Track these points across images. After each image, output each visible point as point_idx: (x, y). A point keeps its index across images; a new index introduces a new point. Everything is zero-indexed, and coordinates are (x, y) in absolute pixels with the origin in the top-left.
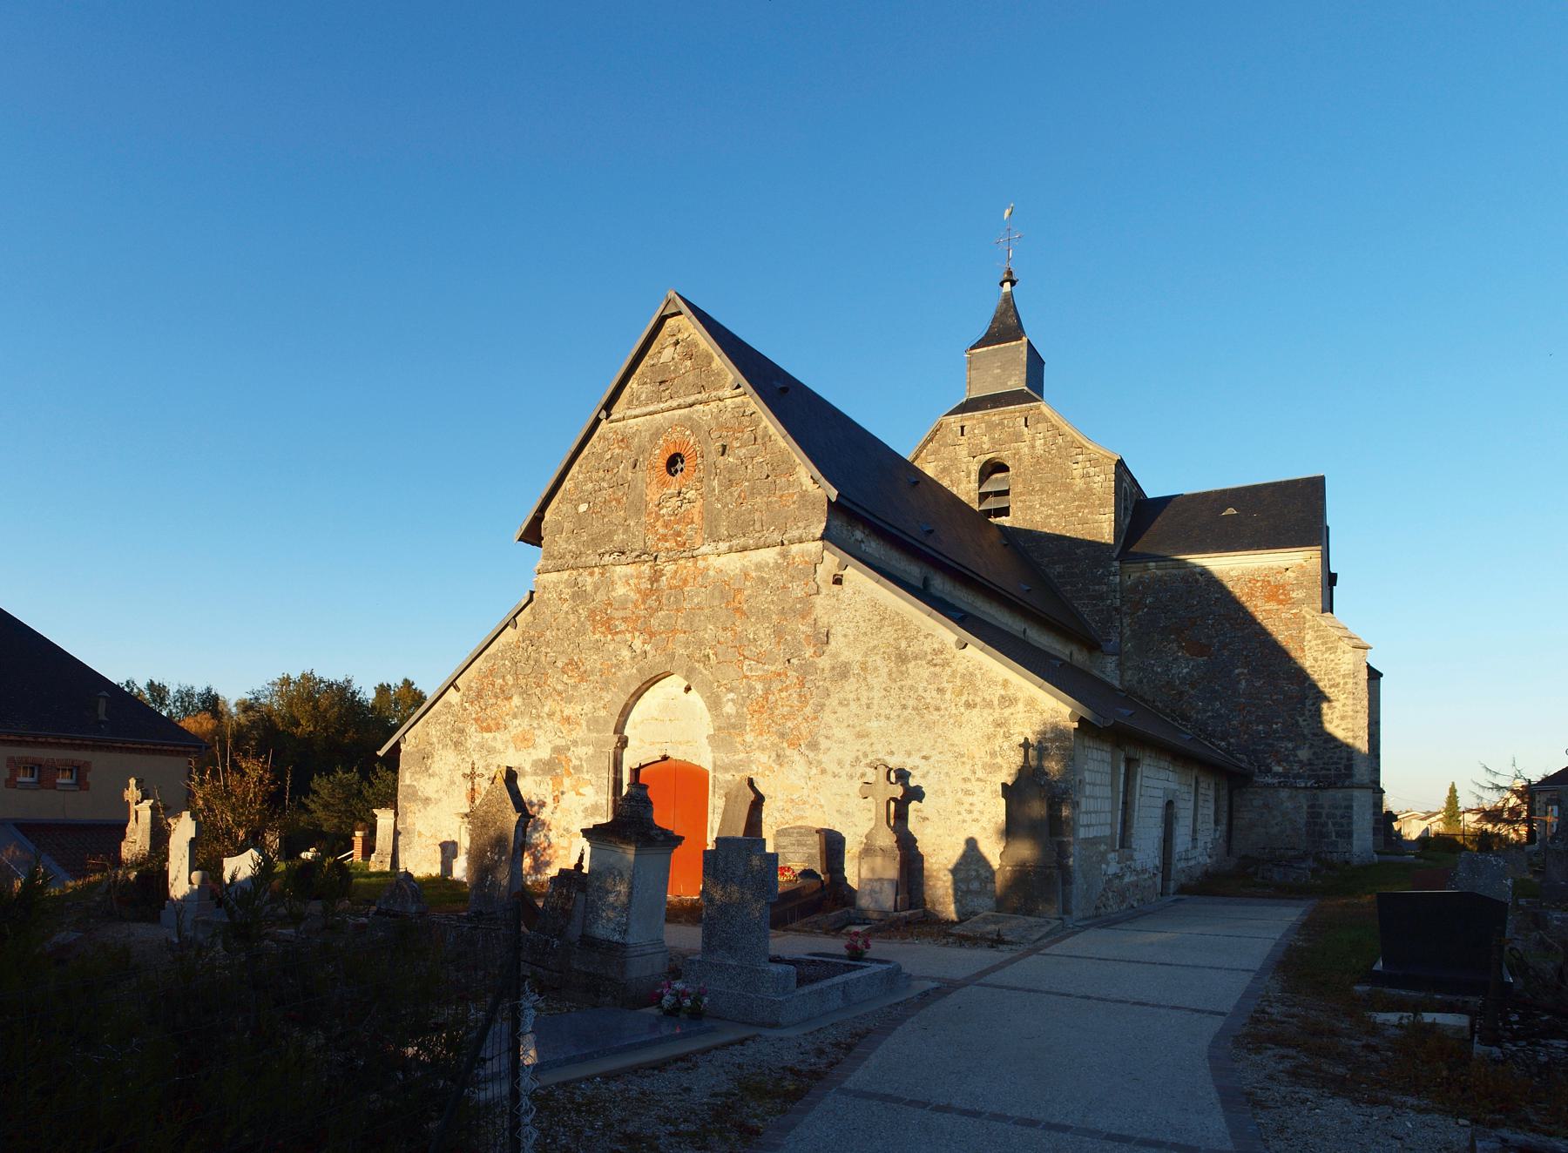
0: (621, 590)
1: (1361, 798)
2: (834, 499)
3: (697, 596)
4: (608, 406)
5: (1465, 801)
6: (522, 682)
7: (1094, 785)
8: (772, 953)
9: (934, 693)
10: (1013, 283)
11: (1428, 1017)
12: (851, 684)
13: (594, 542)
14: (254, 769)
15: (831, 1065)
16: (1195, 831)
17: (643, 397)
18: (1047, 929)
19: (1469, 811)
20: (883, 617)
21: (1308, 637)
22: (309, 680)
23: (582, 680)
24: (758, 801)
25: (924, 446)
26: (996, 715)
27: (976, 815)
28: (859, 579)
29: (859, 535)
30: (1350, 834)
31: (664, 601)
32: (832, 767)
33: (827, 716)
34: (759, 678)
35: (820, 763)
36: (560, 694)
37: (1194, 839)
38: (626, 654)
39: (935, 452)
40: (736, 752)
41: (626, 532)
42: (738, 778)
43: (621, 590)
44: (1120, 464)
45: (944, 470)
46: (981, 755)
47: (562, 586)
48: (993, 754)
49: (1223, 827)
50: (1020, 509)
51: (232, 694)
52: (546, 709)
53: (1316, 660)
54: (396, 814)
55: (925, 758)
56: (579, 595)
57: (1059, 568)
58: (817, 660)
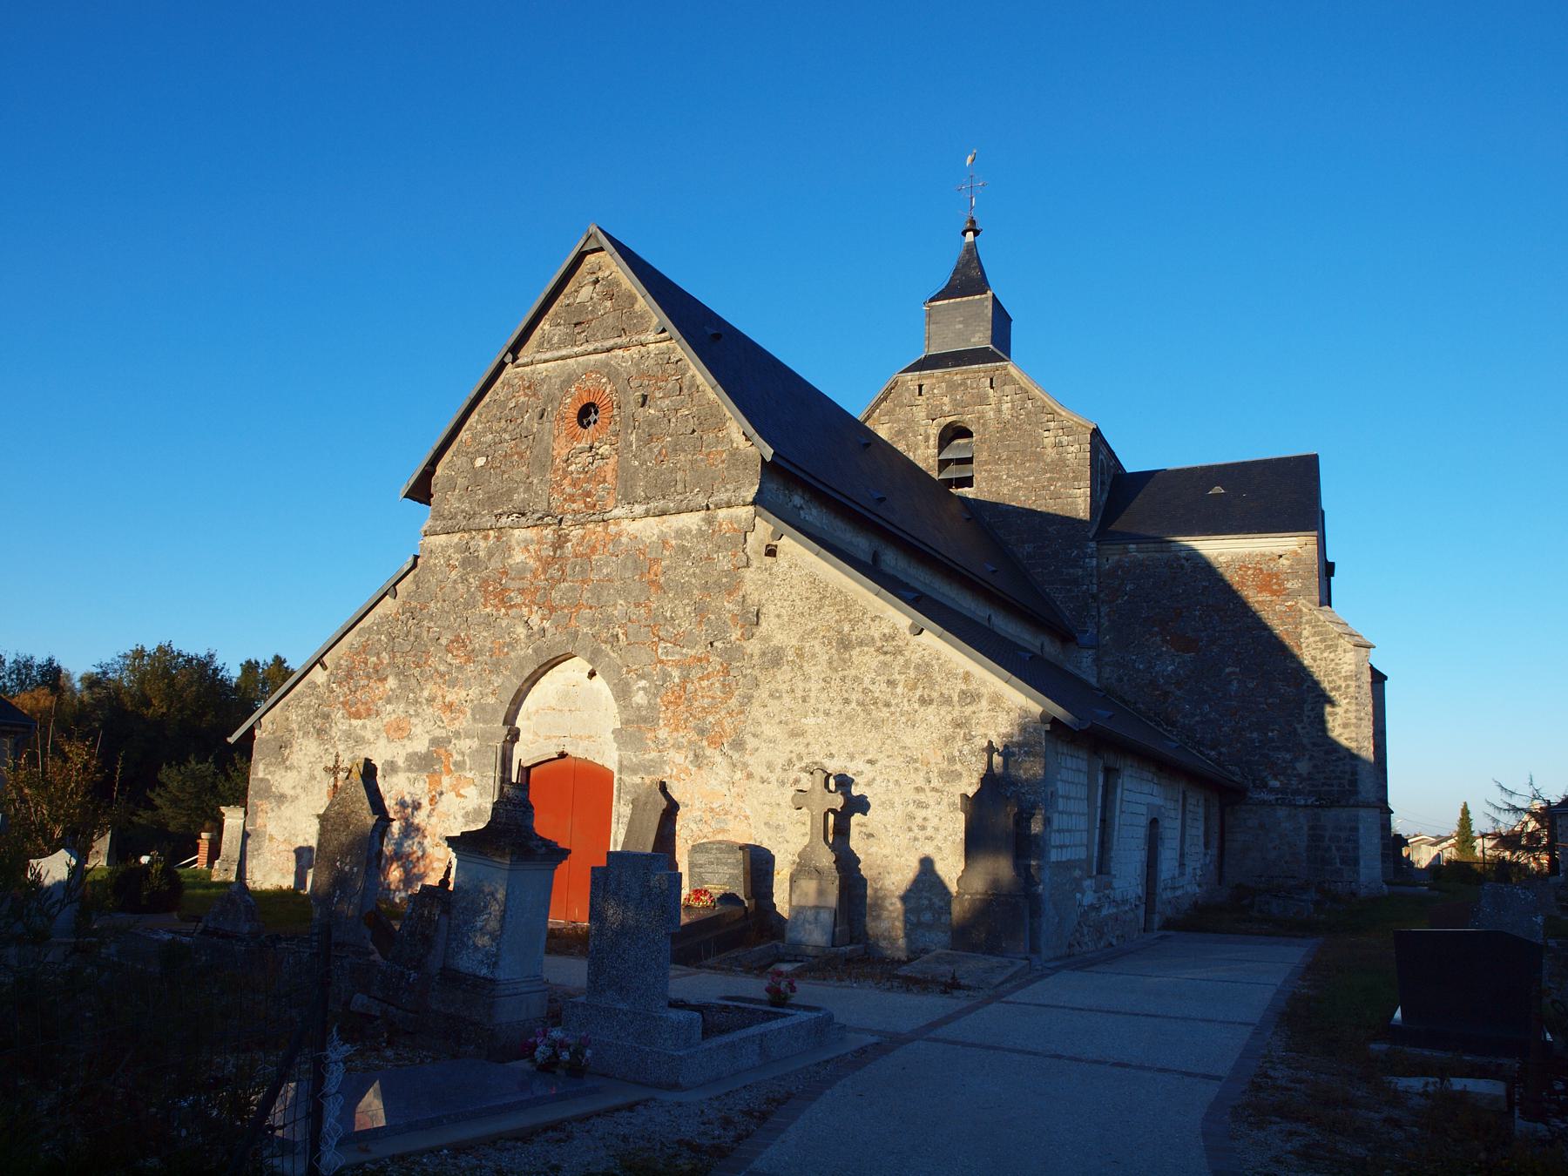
0: (518, 557)
1: (1367, 817)
2: (768, 459)
3: (606, 566)
4: (515, 349)
5: (1480, 824)
6: (399, 660)
7: (1068, 798)
8: (673, 995)
9: (884, 686)
10: (976, 233)
11: (1458, 1084)
12: (784, 674)
13: (491, 501)
14: (78, 753)
15: (739, 1138)
16: (1182, 855)
17: (556, 339)
18: (1011, 971)
19: (1483, 836)
20: (823, 594)
21: (1305, 633)
22: (166, 653)
23: (469, 660)
24: (672, 808)
25: (877, 405)
26: (956, 713)
27: (930, 832)
28: (793, 548)
29: (797, 500)
30: (1356, 862)
31: (568, 570)
32: (759, 771)
33: (756, 711)
34: (677, 664)
35: (745, 765)
36: (442, 675)
37: (1182, 865)
38: (521, 631)
39: (890, 412)
40: (646, 750)
41: (527, 490)
42: (647, 781)
43: (518, 557)
44: (1096, 433)
45: (899, 432)
46: (937, 758)
47: (451, 551)
48: (952, 760)
49: (1214, 851)
50: (986, 480)
51: (78, 665)
52: (426, 694)
53: (1314, 659)
54: (246, 813)
55: (870, 762)
56: (470, 561)
57: (1028, 548)
58: (745, 644)
